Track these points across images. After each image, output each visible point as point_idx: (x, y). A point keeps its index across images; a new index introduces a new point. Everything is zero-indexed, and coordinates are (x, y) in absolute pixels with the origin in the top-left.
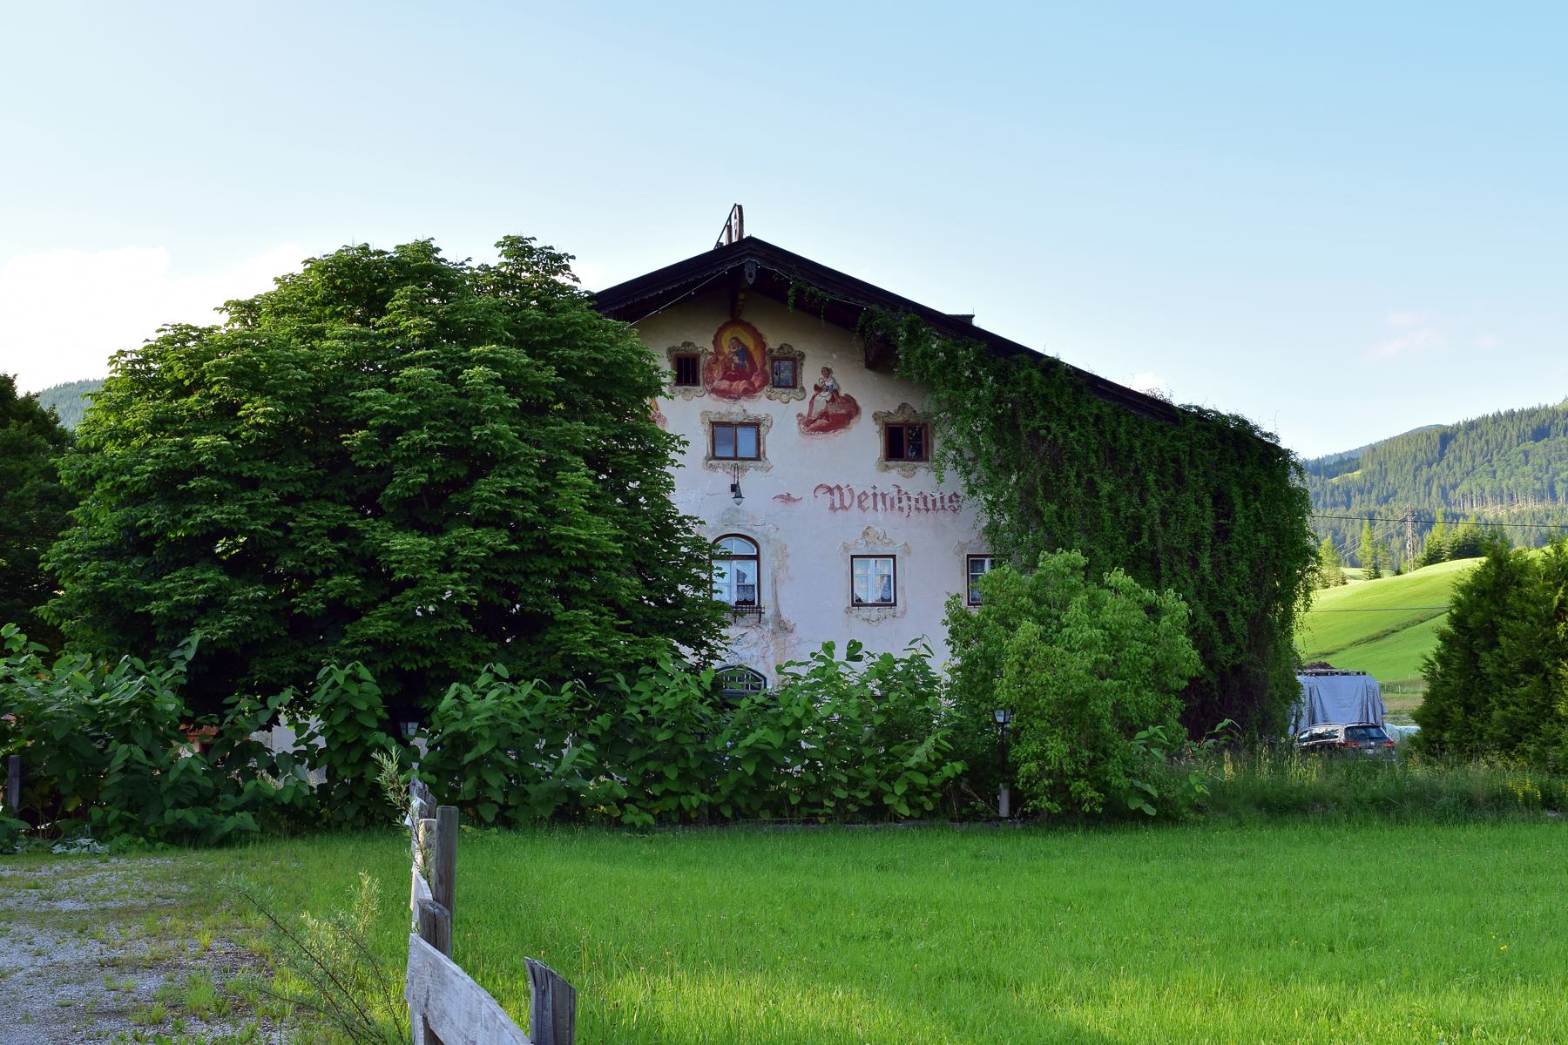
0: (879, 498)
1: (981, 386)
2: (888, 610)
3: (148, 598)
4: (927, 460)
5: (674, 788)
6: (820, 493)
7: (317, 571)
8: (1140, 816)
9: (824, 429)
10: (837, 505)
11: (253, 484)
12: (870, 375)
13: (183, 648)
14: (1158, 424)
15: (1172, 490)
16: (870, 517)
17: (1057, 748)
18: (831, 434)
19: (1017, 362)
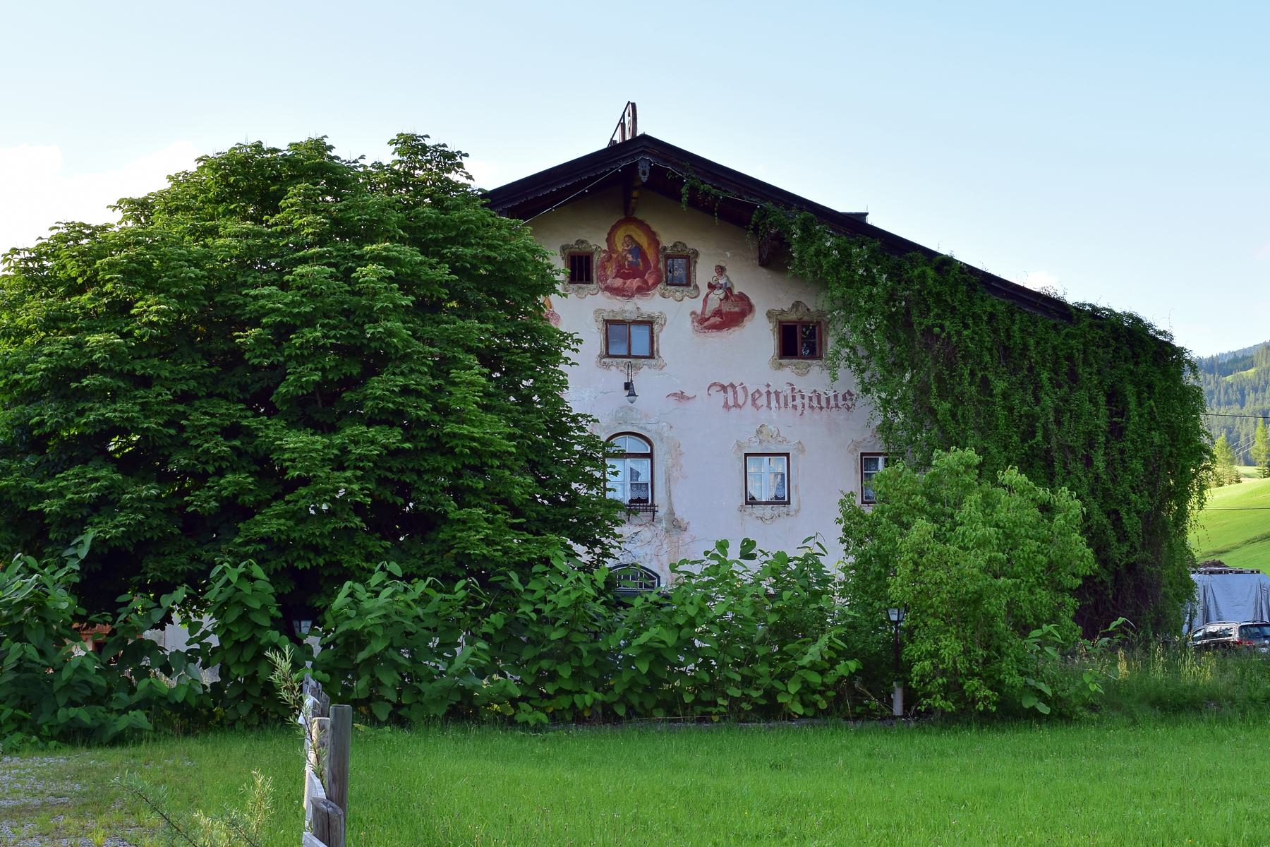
0: (773, 396)
1: (875, 284)
2: (782, 509)
3: (41, 496)
4: (820, 358)
6: (713, 391)
7: (211, 469)
8: (1038, 716)
9: (717, 327)
10: (731, 403)
11: (146, 382)
14: (1052, 322)
15: (1066, 388)
16: (763, 415)
18: (724, 333)
19: (911, 260)
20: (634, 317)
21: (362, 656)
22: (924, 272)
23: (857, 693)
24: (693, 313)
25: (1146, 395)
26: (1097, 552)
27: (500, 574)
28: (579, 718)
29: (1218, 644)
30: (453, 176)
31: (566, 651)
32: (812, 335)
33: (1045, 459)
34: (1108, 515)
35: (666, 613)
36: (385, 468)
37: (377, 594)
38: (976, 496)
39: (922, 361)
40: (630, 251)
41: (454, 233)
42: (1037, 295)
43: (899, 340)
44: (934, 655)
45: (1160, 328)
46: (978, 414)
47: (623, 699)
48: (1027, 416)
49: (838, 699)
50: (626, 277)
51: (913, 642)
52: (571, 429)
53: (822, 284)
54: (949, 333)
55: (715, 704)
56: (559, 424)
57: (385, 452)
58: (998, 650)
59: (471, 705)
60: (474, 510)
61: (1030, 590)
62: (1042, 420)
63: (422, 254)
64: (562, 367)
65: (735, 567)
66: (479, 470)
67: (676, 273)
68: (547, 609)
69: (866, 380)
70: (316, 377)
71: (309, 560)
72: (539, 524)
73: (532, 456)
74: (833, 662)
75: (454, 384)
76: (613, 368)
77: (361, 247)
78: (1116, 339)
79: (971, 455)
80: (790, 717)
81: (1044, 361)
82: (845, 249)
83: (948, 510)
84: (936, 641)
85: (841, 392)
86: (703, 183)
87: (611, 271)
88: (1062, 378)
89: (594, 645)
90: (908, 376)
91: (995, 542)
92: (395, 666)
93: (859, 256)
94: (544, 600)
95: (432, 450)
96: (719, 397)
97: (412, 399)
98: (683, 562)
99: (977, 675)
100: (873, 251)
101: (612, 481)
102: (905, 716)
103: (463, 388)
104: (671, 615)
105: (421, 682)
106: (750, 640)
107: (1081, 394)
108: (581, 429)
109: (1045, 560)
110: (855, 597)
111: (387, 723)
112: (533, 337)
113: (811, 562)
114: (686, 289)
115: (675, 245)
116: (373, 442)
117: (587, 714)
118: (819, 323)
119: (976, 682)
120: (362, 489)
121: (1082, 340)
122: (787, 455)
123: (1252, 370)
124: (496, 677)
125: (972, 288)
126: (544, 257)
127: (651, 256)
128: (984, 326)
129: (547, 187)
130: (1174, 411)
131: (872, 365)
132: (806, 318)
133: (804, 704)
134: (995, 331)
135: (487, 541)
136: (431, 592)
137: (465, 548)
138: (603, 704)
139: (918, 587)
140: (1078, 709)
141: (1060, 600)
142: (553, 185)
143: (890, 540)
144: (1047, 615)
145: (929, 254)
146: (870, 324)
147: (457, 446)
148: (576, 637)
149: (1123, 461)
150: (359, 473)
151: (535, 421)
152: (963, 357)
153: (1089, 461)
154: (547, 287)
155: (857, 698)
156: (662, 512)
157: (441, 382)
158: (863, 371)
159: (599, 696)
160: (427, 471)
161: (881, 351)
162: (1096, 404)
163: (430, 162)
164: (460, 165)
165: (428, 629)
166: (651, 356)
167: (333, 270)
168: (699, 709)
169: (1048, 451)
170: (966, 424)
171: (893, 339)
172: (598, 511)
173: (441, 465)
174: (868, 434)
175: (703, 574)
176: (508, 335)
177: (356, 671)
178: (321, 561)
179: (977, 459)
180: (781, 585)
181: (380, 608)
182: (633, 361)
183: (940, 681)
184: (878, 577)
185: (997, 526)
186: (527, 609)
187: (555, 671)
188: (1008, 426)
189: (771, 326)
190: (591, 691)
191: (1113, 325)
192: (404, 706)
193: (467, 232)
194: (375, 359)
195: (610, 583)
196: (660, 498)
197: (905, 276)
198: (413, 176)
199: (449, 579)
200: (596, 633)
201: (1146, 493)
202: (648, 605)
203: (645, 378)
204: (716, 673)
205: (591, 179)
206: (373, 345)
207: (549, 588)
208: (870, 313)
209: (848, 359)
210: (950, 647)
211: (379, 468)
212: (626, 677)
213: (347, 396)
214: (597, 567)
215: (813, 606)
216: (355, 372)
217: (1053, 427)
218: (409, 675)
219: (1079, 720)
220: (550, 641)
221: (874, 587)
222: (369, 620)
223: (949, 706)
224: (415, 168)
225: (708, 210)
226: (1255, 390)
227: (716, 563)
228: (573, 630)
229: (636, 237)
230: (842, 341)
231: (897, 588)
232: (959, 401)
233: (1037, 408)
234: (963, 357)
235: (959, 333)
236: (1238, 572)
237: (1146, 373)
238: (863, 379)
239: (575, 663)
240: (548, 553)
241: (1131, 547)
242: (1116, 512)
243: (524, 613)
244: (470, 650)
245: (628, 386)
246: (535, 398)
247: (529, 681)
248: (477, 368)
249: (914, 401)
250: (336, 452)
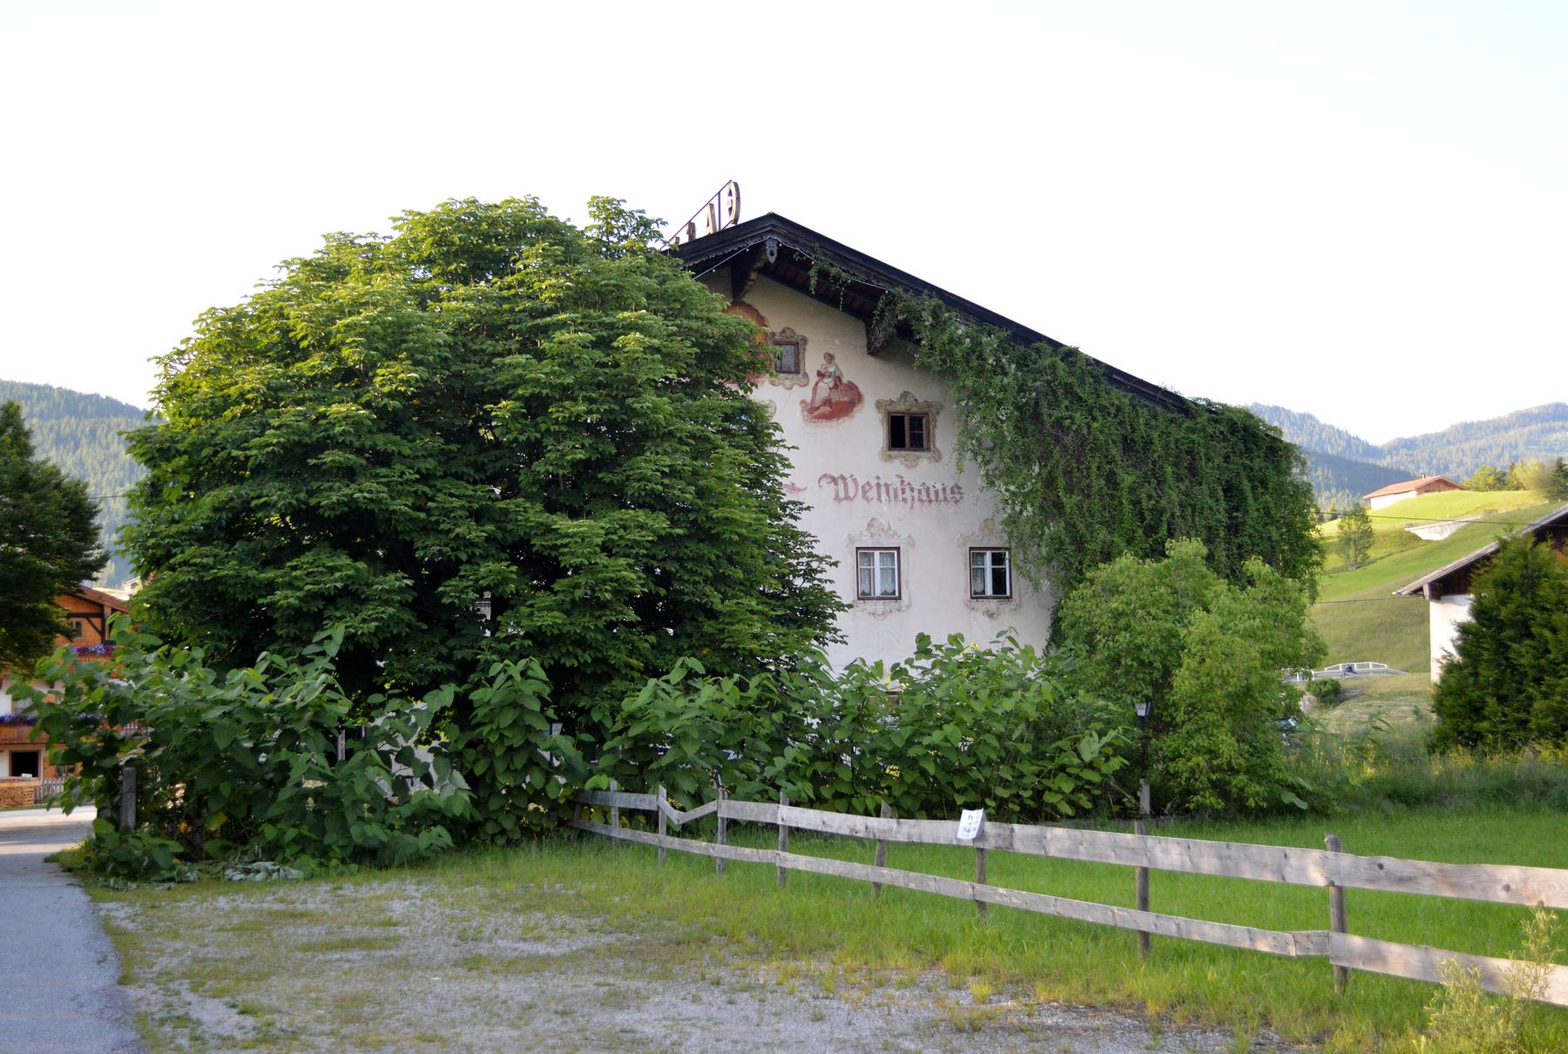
0: (883, 489)
1: (1006, 374)
2: (892, 604)
3: (271, 587)
4: (928, 449)
5: (845, 790)
6: (823, 483)
7: (464, 557)
8: (1292, 809)
9: (828, 417)
10: (842, 495)
11: (384, 459)
12: (872, 359)
13: (320, 643)
14: (1170, 415)
15: (1187, 482)
16: (874, 508)
17: (1227, 745)
18: (834, 423)
19: (1038, 351)
71: (576, 658)
88: (1183, 472)
125: (1097, 380)
132: (914, 409)
145: (1056, 345)
170: (1092, 516)
171: (1020, 429)
205: (718, 258)
235: (1089, 427)
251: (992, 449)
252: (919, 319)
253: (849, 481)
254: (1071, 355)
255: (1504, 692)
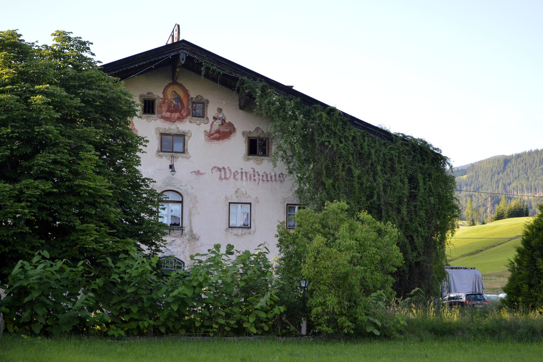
0: (244, 174)
2: (246, 231)
4: (268, 156)
6: (214, 171)
8: (371, 336)
9: (218, 139)
10: (223, 177)
12: (241, 111)
14: (383, 141)
15: (389, 175)
16: (239, 184)
18: (221, 142)
20: (175, 132)
21: (27, 299)
22: (321, 115)
23: (283, 323)
24: (205, 131)
25: (428, 179)
26: (404, 255)
27: (102, 258)
28: (141, 333)
29: (454, 303)
30: (85, 54)
31: (136, 299)
32: (264, 145)
33: (378, 209)
34: (408, 238)
35: (188, 280)
36: (43, 202)
37: (36, 267)
38: (346, 225)
39: (319, 159)
40: (174, 99)
41: (84, 83)
42: (376, 128)
43: (308, 148)
44: (323, 304)
45: (435, 146)
46: (346, 186)
47: (164, 324)
48: (369, 188)
49: (274, 326)
50: (172, 112)
51: (312, 297)
52: (141, 186)
53: (270, 118)
54: (332, 145)
55: (212, 327)
56: (136, 183)
57: (43, 193)
58: (355, 302)
59: (85, 326)
60: (89, 225)
61: (371, 273)
62: (377, 190)
63: (66, 92)
64: (138, 154)
65: (224, 257)
66: (93, 205)
67: (197, 111)
68: (126, 277)
69: (291, 167)
70: (7, 153)
72: (123, 234)
73: (121, 199)
74: (272, 307)
75: (81, 159)
76: (164, 158)
77: (33, 87)
78: (414, 151)
79: (344, 204)
80: (249, 334)
81: (379, 161)
82: (283, 102)
83: (332, 232)
84: (325, 297)
85: (278, 173)
86: (213, 65)
87: (165, 108)
88: (387, 169)
89: (150, 296)
90: (312, 166)
91: (355, 248)
92: (45, 305)
93: (289, 105)
94: (125, 272)
95: (68, 193)
96: (217, 174)
97: (59, 166)
98: (197, 255)
99: (344, 315)
100: (297, 103)
101: (162, 213)
102: (307, 334)
103: (86, 162)
104: (190, 281)
105: (58, 314)
106: (230, 295)
107: (397, 178)
108: (147, 186)
109: (379, 258)
110: (283, 274)
111: (39, 335)
112: (123, 138)
113: (262, 257)
114: (202, 119)
115: (197, 97)
116: (37, 188)
117: (145, 331)
118: (268, 138)
119: (344, 318)
120: (30, 212)
121: (398, 151)
122: (250, 204)
123: (465, 176)
124: (98, 312)
125: (345, 123)
126: (131, 97)
127: (185, 101)
128: (350, 142)
129: (133, 64)
130: (441, 187)
131: (294, 160)
132: (262, 136)
133: (257, 328)
134: (355, 145)
135: (96, 241)
136: (65, 267)
137: (84, 244)
138: (154, 326)
139: (316, 270)
140: (394, 333)
141: (386, 278)
142: (136, 63)
143: (302, 246)
144: (379, 286)
145: (324, 106)
146: (294, 139)
147: (81, 191)
148: (141, 292)
149: (416, 211)
150: (29, 204)
151: (123, 180)
152: (339, 157)
153: (399, 211)
154: (131, 113)
155: (284, 326)
156: (186, 230)
157: (74, 158)
158: (289, 163)
159: (152, 322)
160: (65, 204)
161: (299, 153)
162: (403, 183)
163: (72, 46)
164: (88, 49)
165: (63, 286)
166: (184, 152)
167: (19, 97)
168: (203, 330)
169: (379, 205)
170: (339, 191)
171: (305, 147)
172: (154, 227)
173: (73, 201)
174: (290, 194)
175: (207, 261)
176: (112, 137)
177: (24, 307)
178: (7, 250)
179: (347, 207)
180: (246, 267)
181: (38, 274)
182: (174, 154)
183: (326, 318)
184: (296, 264)
185: (356, 240)
186: (116, 277)
187: (129, 309)
188: (360, 192)
189: (244, 139)
190: (148, 319)
191: (413, 144)
192: (49, 326)
193: (91, 82)
194: (39, 144)
195: (159, 264)
196: (186, 223)
197: (312, 116)
198: (63, 52)
199: (75, 260)
200: (151, 290)
201: (426, 227)
202: (178, 276)
203: (180, 163)
204: (213, 311)
205: (156, 61)
206: (38, 137)
207: (128, 266)
208: (294, 134)
209: (282, 157)
210: (332, 300)
211: (40, 202)
212: (166, 313)
213: (24, 163)
214: (153, 256)
215: (262, 278)
216: (28, 152)
217: (382, 193)
218: (53, 310)
219: (395, 339)
220: (127, 294)
221: (293, 269)
222: (31, 280)
223: (330, 330)
224: (64, 49)
225: (214, 80)
226: (467, 185)
227: (214, 255)
228: (140, 288)
229: (178, 93)
230: (279, 147)
231: (306, 270)
232: (336, 179)
233: (375, 184)
234: (339, 157)
235: (338, 145)
236: (456, 268)
237: (428, 168)
238: (289, 166)
239: (140, 305)
240: (128, 248)
241: (418, 253)
242: (412, 236)
243: (114, 279)
244: (85, 297)
245: (171, 167)
246: (124, 169)
247: (116, 314)
248: (93, 152)
249: (314, 179)
250: (16, 192)
251: (292, 156)
252: (255, 93)
253: (227, 170)
254: (333, 110)
255: (533, 282)
